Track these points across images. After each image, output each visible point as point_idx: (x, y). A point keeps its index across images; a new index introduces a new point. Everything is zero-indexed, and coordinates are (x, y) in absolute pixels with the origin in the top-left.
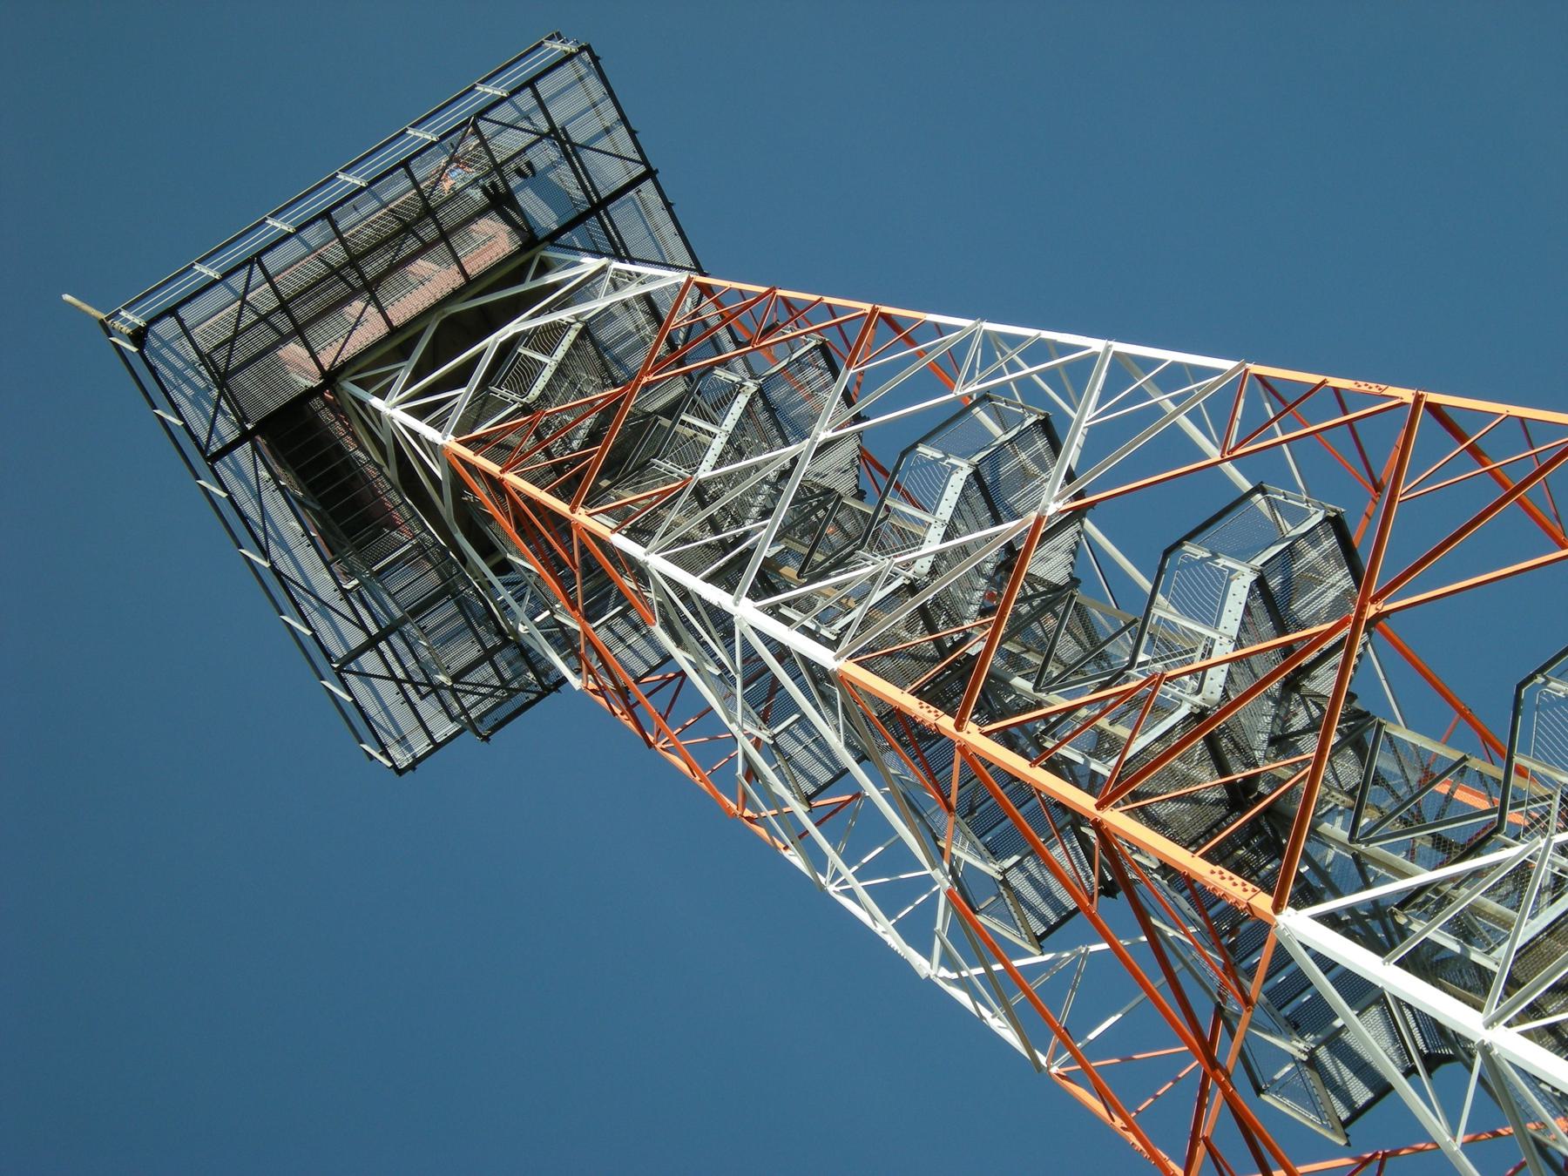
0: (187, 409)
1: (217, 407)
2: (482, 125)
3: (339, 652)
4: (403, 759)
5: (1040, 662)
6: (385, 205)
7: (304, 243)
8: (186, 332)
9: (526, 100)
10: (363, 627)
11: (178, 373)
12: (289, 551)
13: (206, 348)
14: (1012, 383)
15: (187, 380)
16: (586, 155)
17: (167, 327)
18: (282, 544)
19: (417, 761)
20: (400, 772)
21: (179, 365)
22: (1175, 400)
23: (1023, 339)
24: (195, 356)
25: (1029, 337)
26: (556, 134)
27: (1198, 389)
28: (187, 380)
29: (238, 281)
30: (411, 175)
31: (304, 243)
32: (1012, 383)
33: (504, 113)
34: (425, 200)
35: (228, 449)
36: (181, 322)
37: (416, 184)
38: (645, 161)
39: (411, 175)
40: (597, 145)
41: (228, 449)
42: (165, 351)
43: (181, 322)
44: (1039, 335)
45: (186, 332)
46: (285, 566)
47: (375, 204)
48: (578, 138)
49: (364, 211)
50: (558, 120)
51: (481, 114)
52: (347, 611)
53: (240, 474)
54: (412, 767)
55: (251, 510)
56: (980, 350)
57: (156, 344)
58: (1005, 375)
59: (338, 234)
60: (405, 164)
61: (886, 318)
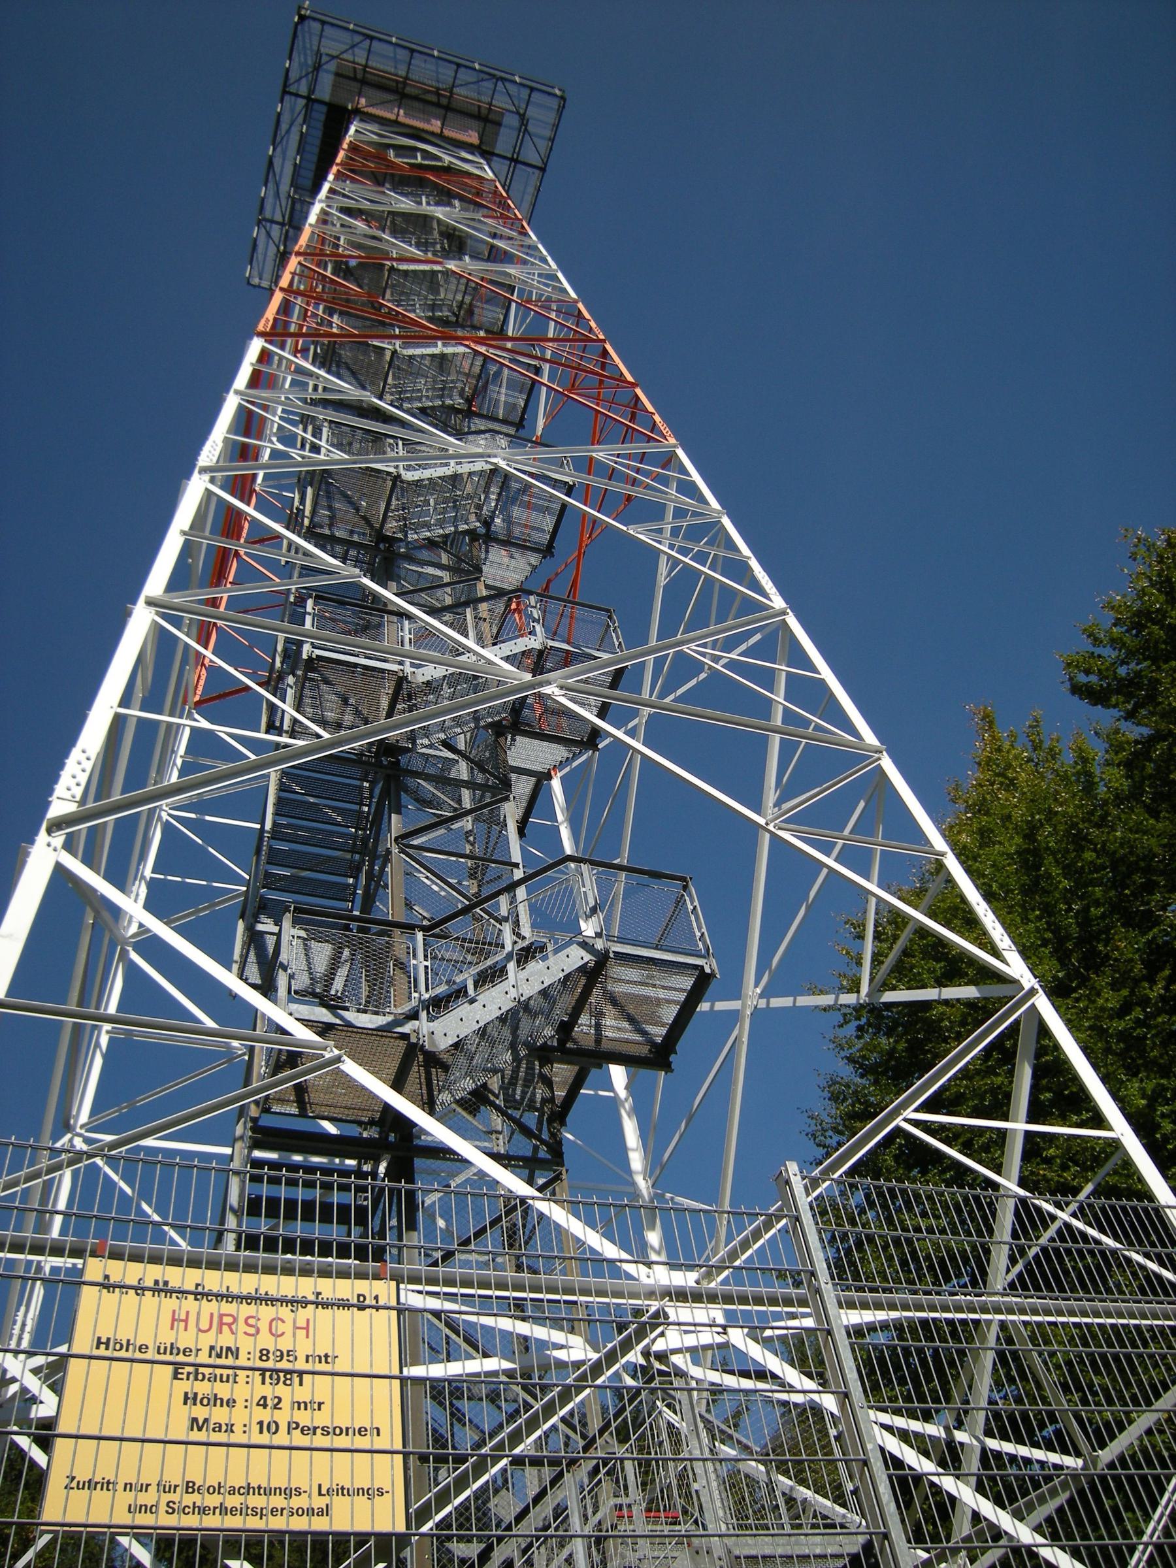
0: (295, 64)
1: (307, 75)
2: (500, 83)
3: (268, 215)
4: (256, 281)
5: (468, 806)
6: (582, 358)
7: (395, 53)
8: (321, 36)
9: (525, 93)
10: (284, 217)
11: (304, 47)
12: (284, 159)
13: (323, 50)
14: (825, 871)
15: (305, 55)
16: (527, 137)
17: (316, 26)
18: (284, 153)
19: (259, 286)
20: (249, 283)
21: (308, 45)
22: (788, 715)
23: (735, 549)
24: (315, 48)
25: (740, 552)
26: (523, 118)
27: (818, 728)
28: (305, 55)
29: (358, 38)
30: (456, 72)
31: (395, 53)
32: (825, 871)
33: (513, 89)
34: (453, 86)
35: (297, 95)
36: (322, 30)
37: (455, 78)
38: (546, 165)
39: (456, 72)
40: (535, 139)
41: (297, 95)
42: (307, 35)
43: (322, 30)
44: (749, 558)
45: (321, 36)
46: (277, 163)
47: (434, 68)
48: (530, 128)
49: (428, 66)
50: (528, 114)
51: (503, 79)
52: (284, 204)
53: (292, 110)
54: (254, 286)
55: (284, 126)
56: (758, 637)
57: (306, 29)
58: (828, 855)
59: (410, 64)
60: (459, 65)
61: (605, 353)
